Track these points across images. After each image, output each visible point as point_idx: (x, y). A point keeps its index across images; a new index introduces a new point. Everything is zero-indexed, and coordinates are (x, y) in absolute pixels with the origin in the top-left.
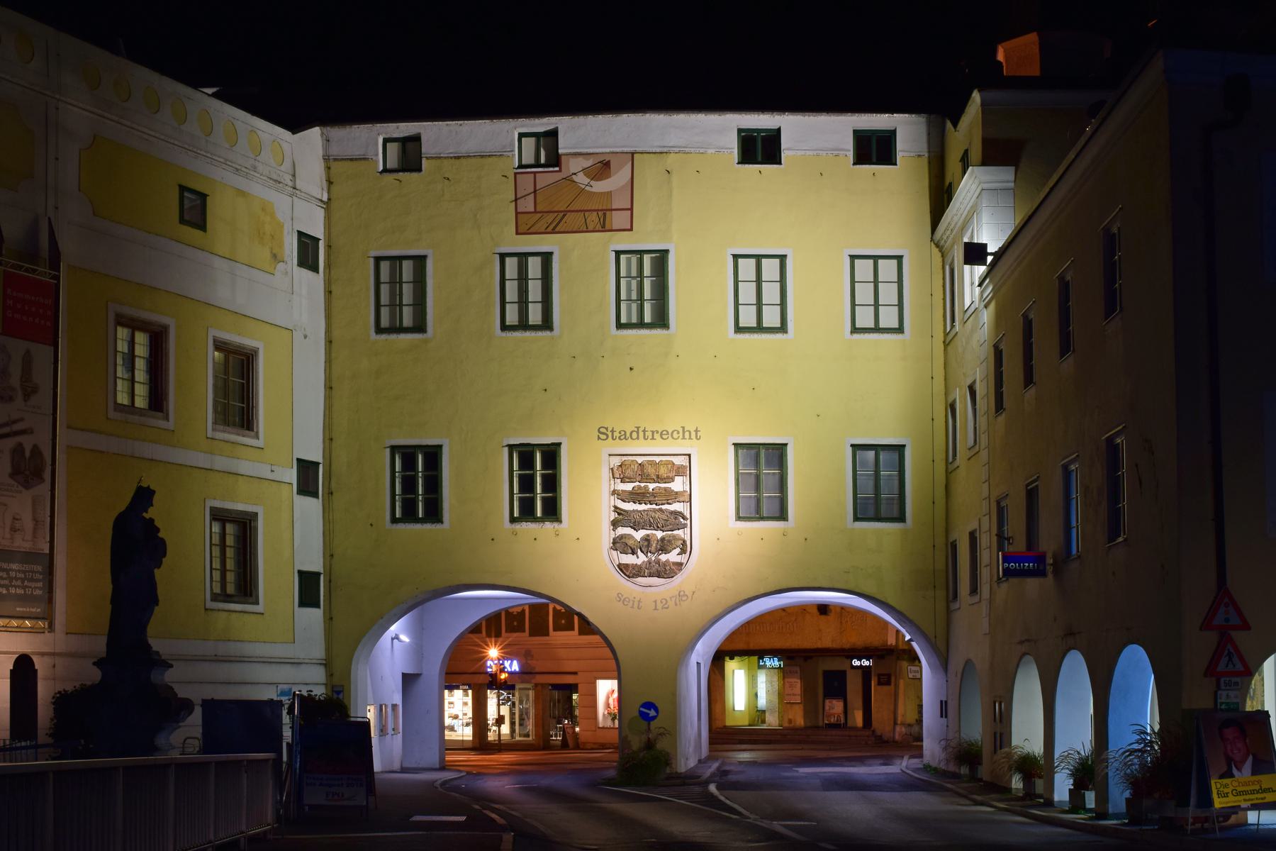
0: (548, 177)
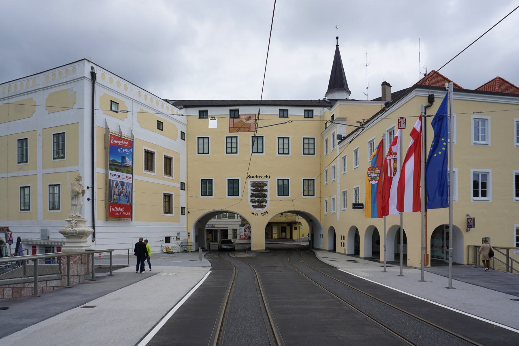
0: (236, 120)
